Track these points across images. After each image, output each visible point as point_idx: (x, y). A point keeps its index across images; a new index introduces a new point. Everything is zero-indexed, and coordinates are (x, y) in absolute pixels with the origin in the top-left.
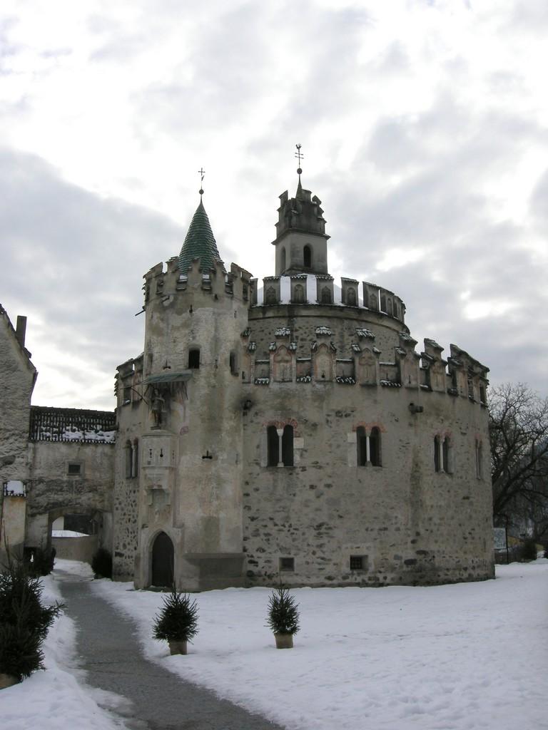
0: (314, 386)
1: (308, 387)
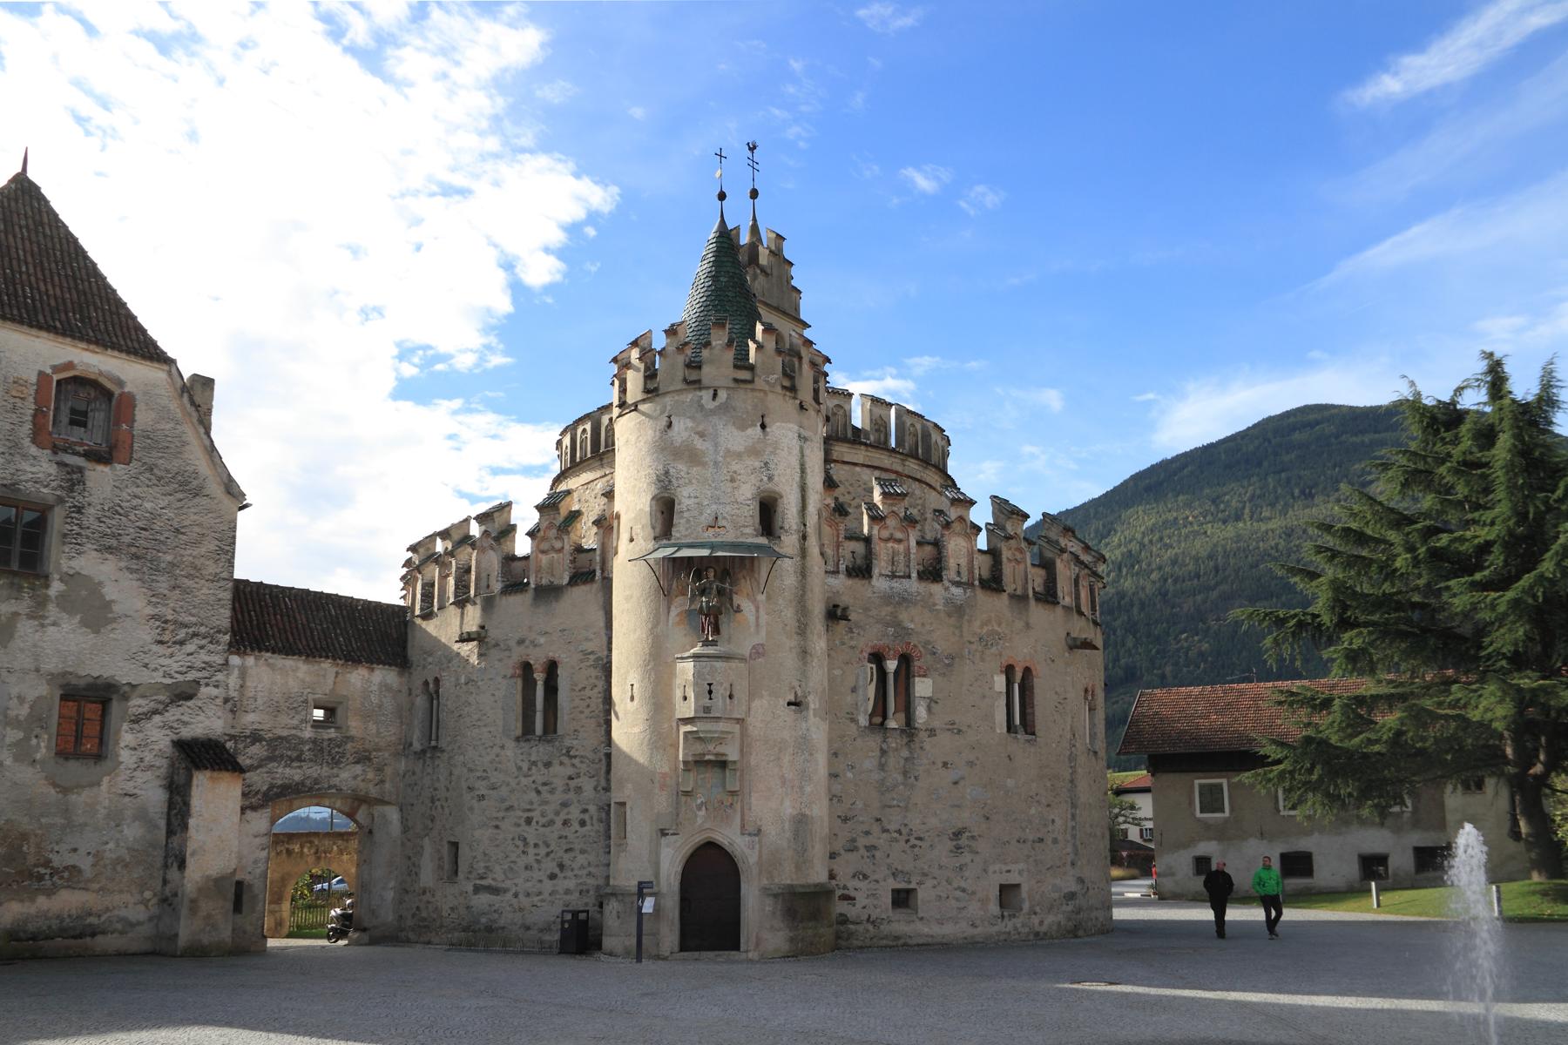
0: (947, 589)
1: (936, 588)
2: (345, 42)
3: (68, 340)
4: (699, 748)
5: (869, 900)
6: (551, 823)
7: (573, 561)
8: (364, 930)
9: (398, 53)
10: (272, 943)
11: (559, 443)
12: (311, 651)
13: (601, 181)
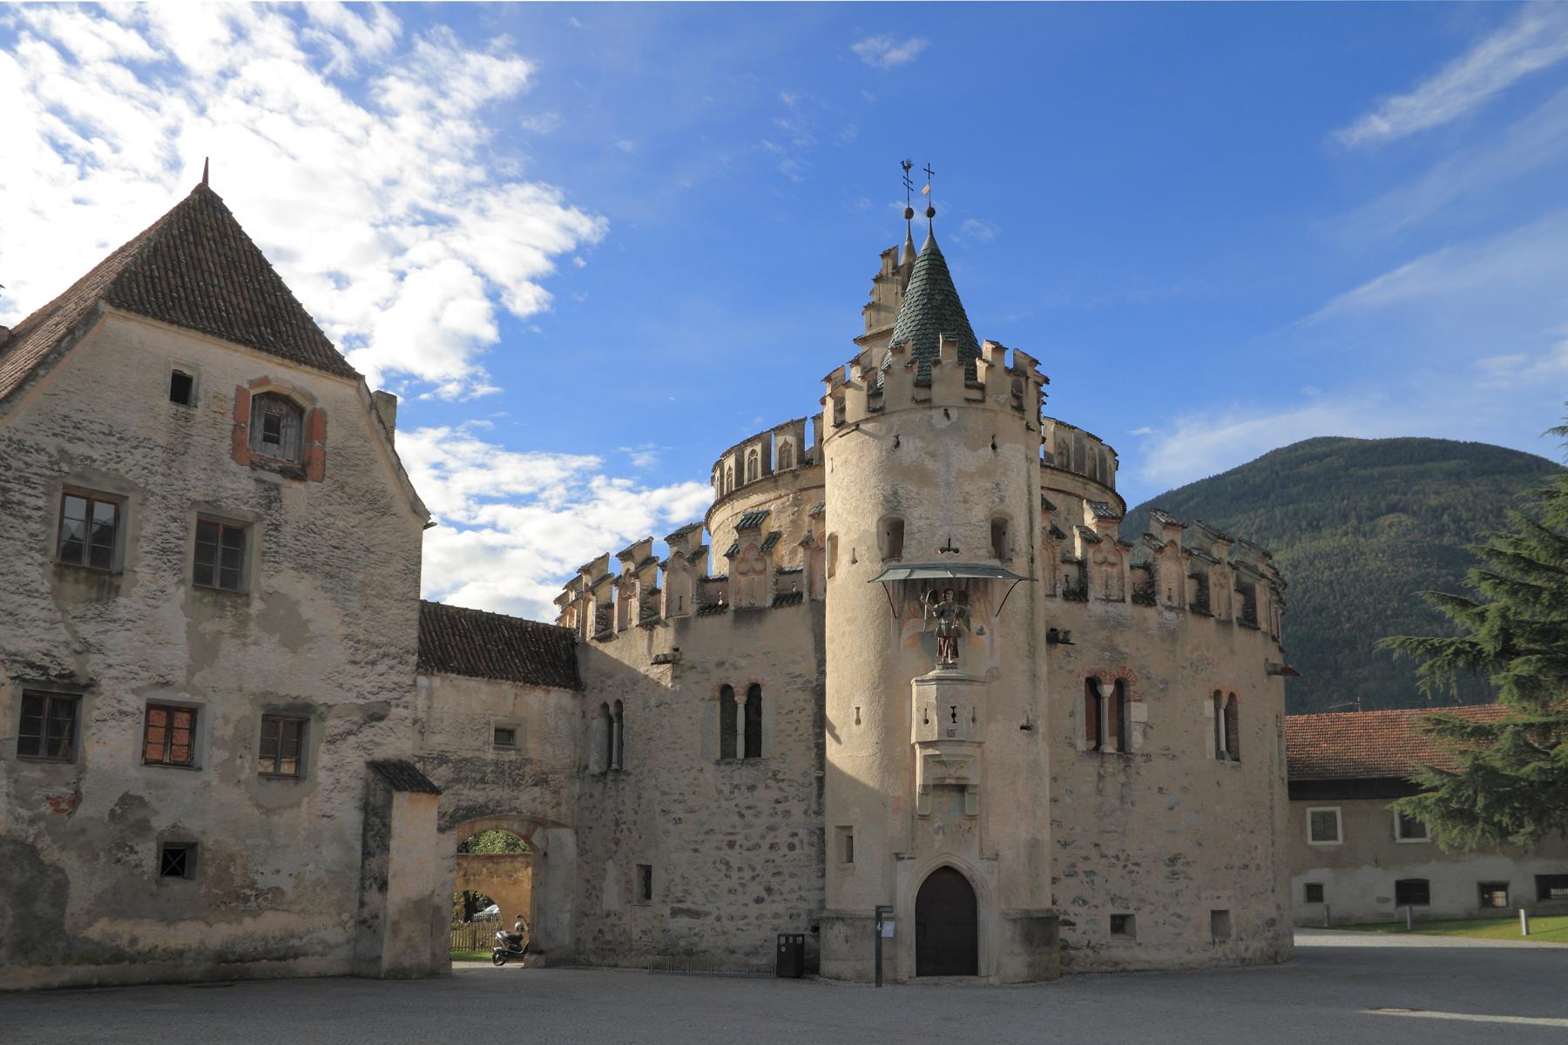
0: (1160, 614)
1: (1150, 612)
2: (327, 71)
3: (264, 354)
4: (939, 771)
5: (1088, 927)
6: (757, 846)
7: (776, 583)
8: (541, 953)
9: (381, 82)
10: (456, 965)
11: (719, 464)
12: (493, 672)
13: (589, 209)
